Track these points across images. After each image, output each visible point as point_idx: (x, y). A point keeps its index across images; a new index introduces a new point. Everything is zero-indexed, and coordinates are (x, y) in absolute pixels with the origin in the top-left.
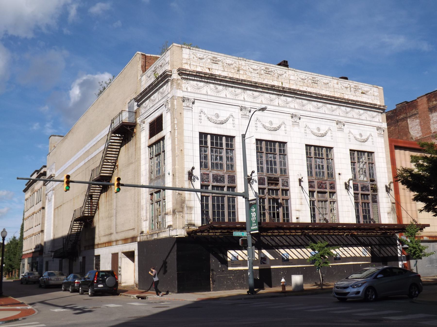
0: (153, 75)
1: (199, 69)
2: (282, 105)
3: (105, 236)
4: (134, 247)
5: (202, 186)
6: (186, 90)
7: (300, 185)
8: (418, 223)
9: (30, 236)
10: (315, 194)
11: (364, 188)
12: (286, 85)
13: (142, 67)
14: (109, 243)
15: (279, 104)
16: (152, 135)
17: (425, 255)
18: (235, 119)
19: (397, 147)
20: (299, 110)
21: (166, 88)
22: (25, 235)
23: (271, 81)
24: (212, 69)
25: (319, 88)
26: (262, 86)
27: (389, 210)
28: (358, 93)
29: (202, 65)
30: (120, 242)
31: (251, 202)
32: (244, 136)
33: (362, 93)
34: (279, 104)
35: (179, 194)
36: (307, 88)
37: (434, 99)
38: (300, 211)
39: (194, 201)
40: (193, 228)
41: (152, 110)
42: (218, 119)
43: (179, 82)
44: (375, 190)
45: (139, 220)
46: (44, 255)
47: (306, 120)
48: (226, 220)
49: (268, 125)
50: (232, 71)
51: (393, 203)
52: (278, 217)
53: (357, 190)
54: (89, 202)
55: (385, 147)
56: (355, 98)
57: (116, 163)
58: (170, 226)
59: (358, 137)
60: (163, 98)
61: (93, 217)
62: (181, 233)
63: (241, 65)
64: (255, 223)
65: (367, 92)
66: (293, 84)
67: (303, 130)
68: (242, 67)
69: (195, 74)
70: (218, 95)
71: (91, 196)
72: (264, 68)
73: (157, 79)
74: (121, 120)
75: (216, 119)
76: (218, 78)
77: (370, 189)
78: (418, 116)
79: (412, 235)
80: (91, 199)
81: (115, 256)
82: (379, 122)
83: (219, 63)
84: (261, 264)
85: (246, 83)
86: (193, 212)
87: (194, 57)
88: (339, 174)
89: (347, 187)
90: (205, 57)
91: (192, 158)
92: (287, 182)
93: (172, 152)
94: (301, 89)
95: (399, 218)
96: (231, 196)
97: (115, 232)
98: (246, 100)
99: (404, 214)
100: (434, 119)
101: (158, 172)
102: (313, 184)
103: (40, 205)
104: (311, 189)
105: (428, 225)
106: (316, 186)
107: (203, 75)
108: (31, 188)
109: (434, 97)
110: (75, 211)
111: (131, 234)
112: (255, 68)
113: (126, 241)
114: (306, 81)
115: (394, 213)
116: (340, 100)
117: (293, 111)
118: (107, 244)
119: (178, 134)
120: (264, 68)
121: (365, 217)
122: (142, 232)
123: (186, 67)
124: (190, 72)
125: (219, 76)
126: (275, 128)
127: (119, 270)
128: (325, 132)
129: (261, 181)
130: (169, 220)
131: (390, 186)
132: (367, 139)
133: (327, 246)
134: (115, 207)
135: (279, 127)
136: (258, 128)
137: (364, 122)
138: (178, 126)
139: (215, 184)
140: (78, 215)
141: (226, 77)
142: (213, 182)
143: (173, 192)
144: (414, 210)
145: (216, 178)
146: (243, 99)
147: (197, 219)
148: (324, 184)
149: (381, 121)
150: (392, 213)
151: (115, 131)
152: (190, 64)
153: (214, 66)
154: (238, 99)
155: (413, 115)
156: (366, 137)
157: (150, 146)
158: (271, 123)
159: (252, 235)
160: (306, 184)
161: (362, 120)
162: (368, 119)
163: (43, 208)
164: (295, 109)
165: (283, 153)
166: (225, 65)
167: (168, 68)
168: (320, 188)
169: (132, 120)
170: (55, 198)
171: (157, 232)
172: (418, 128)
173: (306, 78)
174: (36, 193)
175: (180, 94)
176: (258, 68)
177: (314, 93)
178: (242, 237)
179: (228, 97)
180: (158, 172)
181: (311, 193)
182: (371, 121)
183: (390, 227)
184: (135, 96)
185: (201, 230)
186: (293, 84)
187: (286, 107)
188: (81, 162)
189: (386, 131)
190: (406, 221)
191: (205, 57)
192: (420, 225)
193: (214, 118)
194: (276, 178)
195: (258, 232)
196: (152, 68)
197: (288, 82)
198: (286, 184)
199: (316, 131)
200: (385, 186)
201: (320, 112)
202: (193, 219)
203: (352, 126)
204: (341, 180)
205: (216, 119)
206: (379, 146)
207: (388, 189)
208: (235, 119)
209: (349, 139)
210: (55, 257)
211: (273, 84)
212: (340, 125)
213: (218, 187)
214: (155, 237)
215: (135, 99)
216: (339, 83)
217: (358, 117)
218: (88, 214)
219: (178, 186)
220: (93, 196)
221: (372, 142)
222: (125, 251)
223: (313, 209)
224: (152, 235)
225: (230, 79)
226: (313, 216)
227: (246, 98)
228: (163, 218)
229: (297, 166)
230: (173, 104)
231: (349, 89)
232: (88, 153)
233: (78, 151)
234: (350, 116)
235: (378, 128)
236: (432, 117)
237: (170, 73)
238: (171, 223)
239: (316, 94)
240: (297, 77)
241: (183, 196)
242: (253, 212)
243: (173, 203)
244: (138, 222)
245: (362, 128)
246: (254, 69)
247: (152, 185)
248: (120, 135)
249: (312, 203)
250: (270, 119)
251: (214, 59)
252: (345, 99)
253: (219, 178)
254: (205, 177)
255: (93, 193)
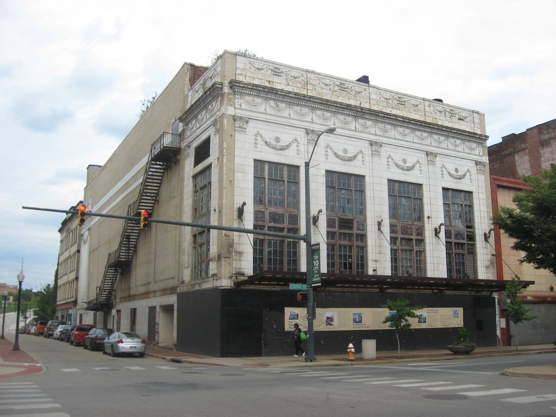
0: (201, 89)
1: (257, 82)
2: (360, 129)
3: (142, 285)
4: (172, 300)
5: (255, 227)
6: (239, 107)
7: (379, 229)
8: (521, 280)
9: (64, 284)
10: (398, 242)
11: (458, 235)
12: (366, 105)
13: (190, 79)
14: (146, 295)
15: (355, 128)
16: (197, 163)
17: (526, 319)
18: (299, 145)
19: (499, 186)
20: (380, 136)
21: (215, 105)
22: (60, 282)
23: (347, 99)
24: (273, 82)
25: (406, 110)
26: (335, 105)
27: (487, 263)
28: (455, 119)
29: (261, 78)
30: (158, 294)
31: (313, 248)
32: (307, 165)
33: (459, 119)
34: (355, 128)
35: (226, 235)
36: (391, 109)
37: (546, 132)
38: (379, 260)
39: (246, 245)
40: (243, 278)
41: (199, 131)
42: (279, 144)
43: (231, 97)
44: (471, 238)
45: (180, 267)
46: (78, 307)
47: (390, 150)
48: (285, 269)
49: (341, 153)
50: (298, 86)
51: (493, 255)
52: (350, 268)
53: (450, 238)
54: (124, 244)
55: (486, 186)
56: (450, 125)
57: (156, 197)
58: (214, 275)
59: (453, 172)
60: (211, 117)
61: (130, 262)
62: (226, 283)
63: (311, 79)
64: (317, 274)
65: (465, 118)
66: (374, 104)
67: (384, 161)
68: (311, 81)
69: (251, 87)
70: (279, 114)
71: (128, 237)
72: (339, 83)
73: (206, 92)
74: (162, 143)
75: (276, 144)
76: (280, 93)
77: (465, 237)
78: (527, 151)
79: (513, 295)
80: (129, 241)
81: (152, 309)
82: (480, 156)
83: (283, 75)
84: (327, 325)
85: (315, 100)
86: (243, 258)
87: (251, 66)
88: (429, 217)
89: (437, 232)
90: (265, 67)
91: (244, 191)
92: (363, 225)
93: (219, 182)
94: (384, 110)
95: (500, 272)
96: (291, 240)
97: (153, 282)
98: (315, 121)
99: (505, 268)
100: (545, 155)
101: (201, 209)
102: (395, 229)
103: (74, 249)
104: (393, 235)
105: (533, 283)
106: (399, 231)
107: (262, 89)
108: (66, 228)
109: (546, 129)
110: (109, 255)
111: (171, 283)
112: (327, 83)
113: (165, 292)
114: (390, 101)
115: (493, 267)
116: (432, 126)
117: (373, 138)
118: (144, 296)
119: (227, 160)
120: (339, 83)
121: (458, 271)
122: (183, 282)
123: (240, 78)
124: (244, 84)
125: (282, 91)
126: (350, 157)
127: (157, 326)
128: (412, 164)
129: (330, 223)
130: (213, 267)
131: (489, 233)
132: (464, 175)
133: (407, 306)
134: (153, 251)
135: (355, 157)
136: (328, 157)
137: (461, 155)
138: (228, 151)
139: (272, 224)
140: (112, 261)
141: (290, 92)
142: (269, 222)
143: (218, 233)
144: (518, 266)
145: (275, 217)
146: (310, 120)
147: (247, 267)
148: (409, 229)
149: (481, 154)
150: (491, 267)
151: (156, 158)
152: (245, 76)
153: (276, 79)
154: (305, 119)
155: (521, 150)
156: (463, 173)
157: (195, 177)
158: (345, 151)
159: (315, 289)
160: (386, 229)
161: (459, 151)
162: (465, 151)
163: (79, 251)
164: (376, 135)
165: (362, 192)
166: (290, 78)
167: (218, 79)
168: (404, 234)
169: (176, 145)
170: (90, 240)
171: (199, 282)
172: (528, 165)
173: (391, 97)
174: (71, 234)
175: (231, 111)
176: (332, 83)
177: (400, 117)
178: (300, 290)
179: (292, 117)
180: (201, 209)
181: (393, 240)
182: (469, 154)
183: (488, 285)
184: (179, 115)
185: (251, 280)
186: (374, 104)
187: (365, 133)
188: (119, 196)
189: (488, 167)
190: (507, 277)
191: (265, 67)
192: (523, 282)
193: (273, 142)
194: (350, 220)
195: (320, 284)
196: (201, 81)
197: (368, 102)
198: (361, 228)
199: (401, 163)
200: (483, 234)
201: (407, 140)
202: (243, 267)
203: (446, 159)
204: (430, 225)
205: (276, 144)
206: (478, 185)
207: (486, 238)
208: (299, 145)
209: (443, 174)
210: (88, 309)
211: (349, 103)
212: (430, 158)
213: (275, 229)
214: (197, 288)
215: (180, 119)
216: (432, 106)
217: (453, 148)
218: (125, 258)
219: (225, 224)
220: (131, 237)
221: (471, 179)
222: (163, 304)
223: (394, 260)
224: (194, 285)
225: (295, 95)
226: (394, 268)
227: (314, 118)
228: (208, 265)
229: (377, 207)
230: (222, 124)
231: (443, 113)
232: (127, 185)
233: (116, 183)
234: (443, 146)
235: (477, 163)
236: (544, 154)
237: (220, 86)
238: (215, 271)
239: (402, 117)
240: (379, 96)
241: (231, 238)
242: (315, 260)
243: (218, 247)
244: (179, 269)
245: (458, 161)
246: (326, 85)
247: (196, 223)
248: (161, 163)
249: (394, 252)
250: (344, 147)
251: (276, 70)
252: (438, 125)
253: (277, 217)
254: (260, 215)
255: (131, 234)
